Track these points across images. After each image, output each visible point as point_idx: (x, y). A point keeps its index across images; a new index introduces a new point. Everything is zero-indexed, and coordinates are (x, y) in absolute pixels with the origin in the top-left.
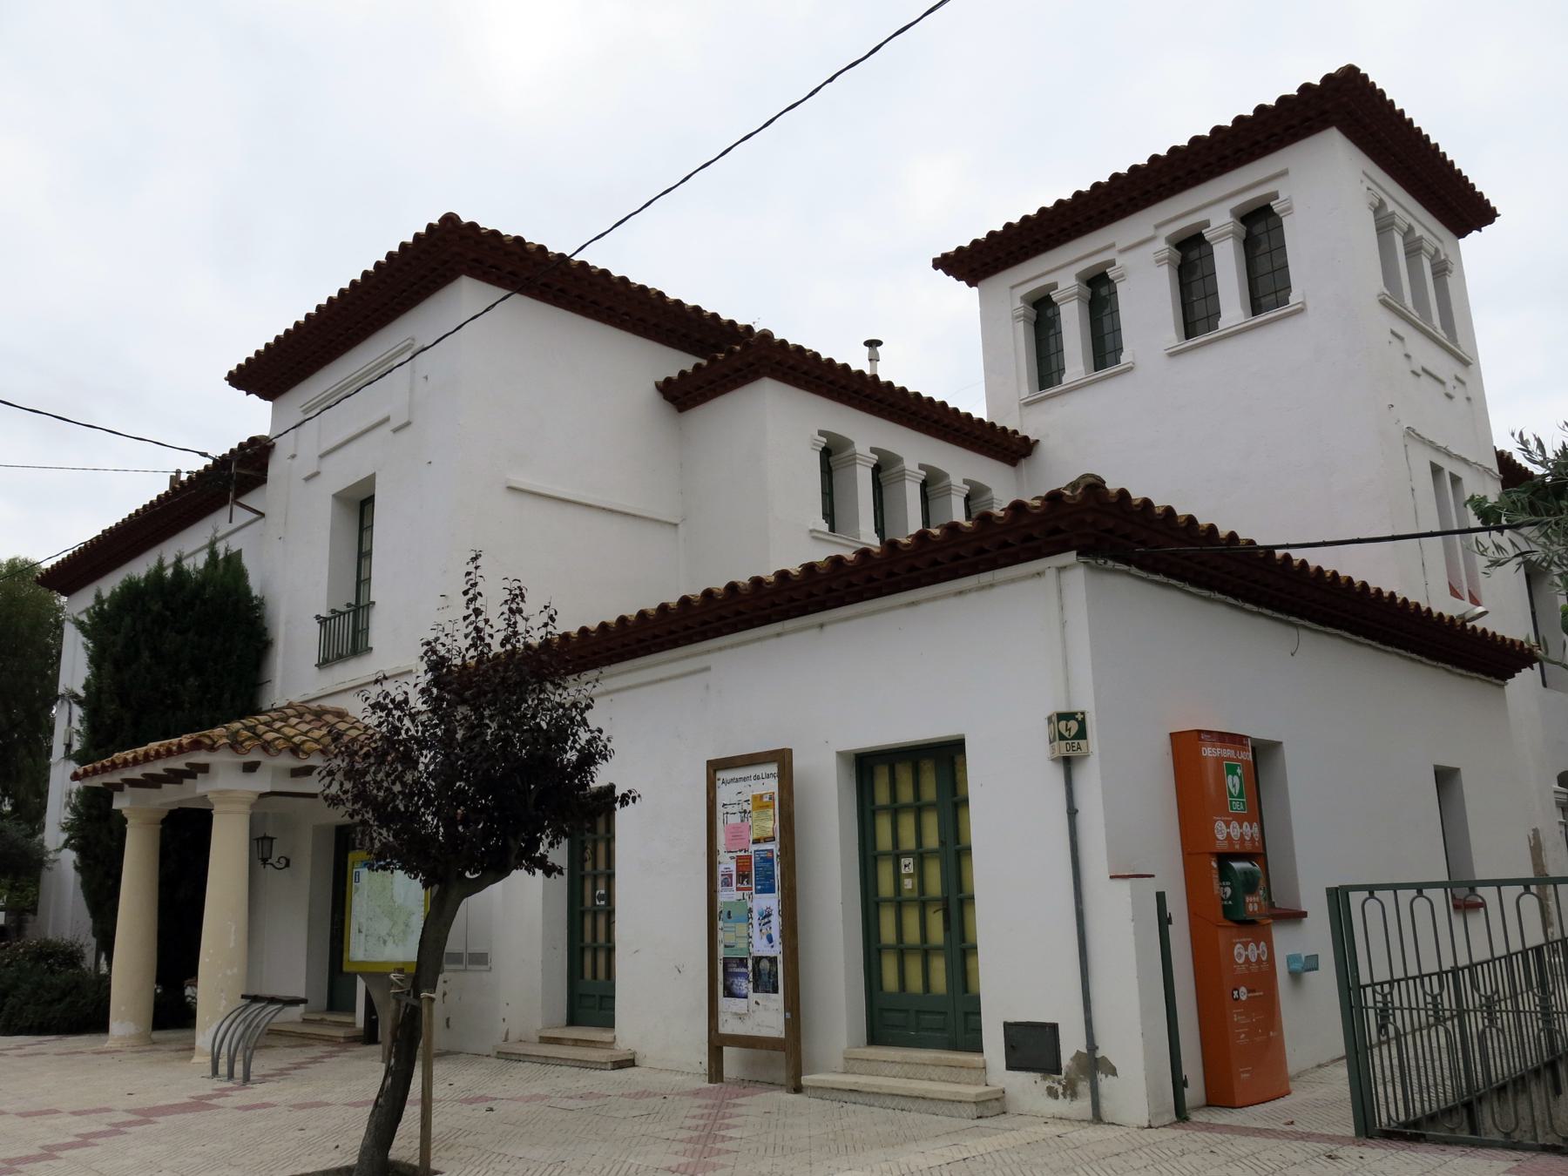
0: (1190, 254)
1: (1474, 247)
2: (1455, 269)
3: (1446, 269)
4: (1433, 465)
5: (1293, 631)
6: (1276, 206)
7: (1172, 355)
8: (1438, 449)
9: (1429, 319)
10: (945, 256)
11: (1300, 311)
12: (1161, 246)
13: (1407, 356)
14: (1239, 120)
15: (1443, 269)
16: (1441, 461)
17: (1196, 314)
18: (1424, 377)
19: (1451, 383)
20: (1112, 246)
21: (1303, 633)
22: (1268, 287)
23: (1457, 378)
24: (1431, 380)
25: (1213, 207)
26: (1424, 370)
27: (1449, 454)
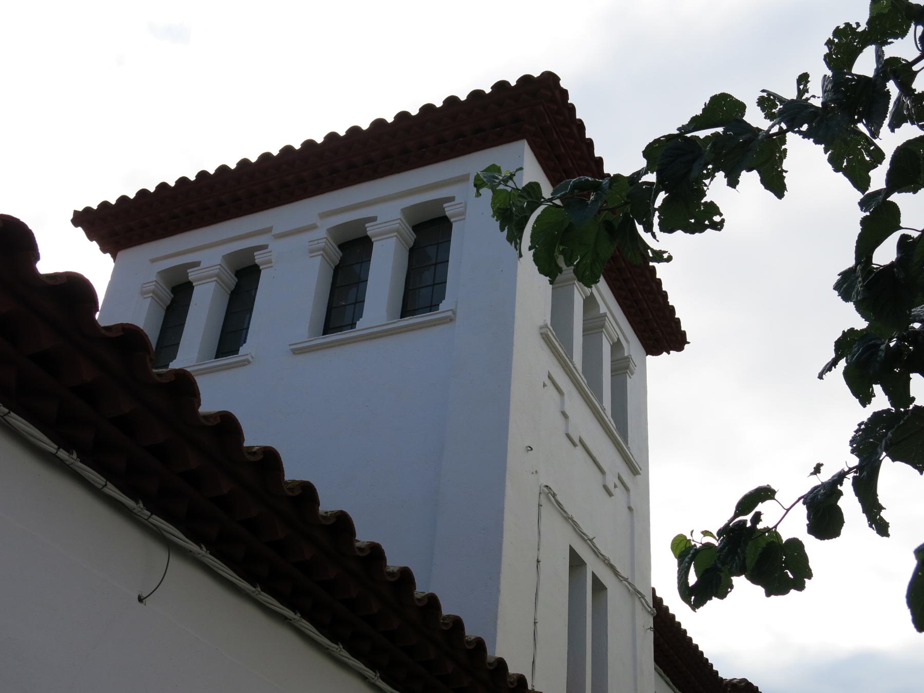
0: (352, 251)
1: (659, 367)
2: (637, 370)
3: (627, 367)
4: (573, 554)
5: (159, 554)
6: (449, 210)
7: (298, 351)
8: (582, 535)
9: (601, 400)
10: (88, 210)
11: (451, 320)
12: (321, 234)
13: (564, 414)
14: (428, 109)
15: (622, 368)
16: (584, 552)
17: (340, 309)
18: (580, 447)
19: (611, 481)
20: (268, 230)
21: (181, 570)
22: (422, 291)
23: (620, 478)
24: (585, 454)
25: (384, 205)
26: (581, 441)
27: (596, 552)
